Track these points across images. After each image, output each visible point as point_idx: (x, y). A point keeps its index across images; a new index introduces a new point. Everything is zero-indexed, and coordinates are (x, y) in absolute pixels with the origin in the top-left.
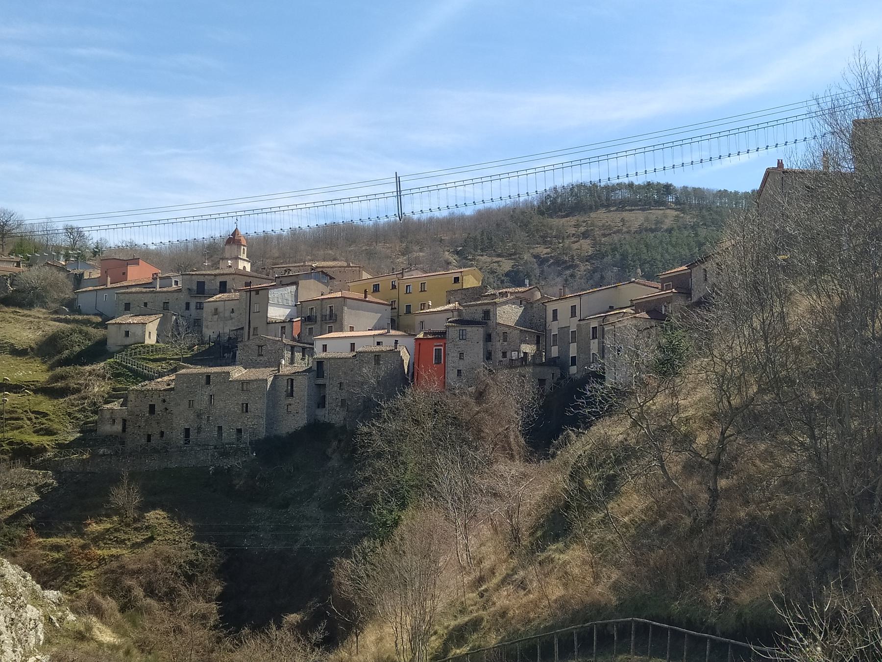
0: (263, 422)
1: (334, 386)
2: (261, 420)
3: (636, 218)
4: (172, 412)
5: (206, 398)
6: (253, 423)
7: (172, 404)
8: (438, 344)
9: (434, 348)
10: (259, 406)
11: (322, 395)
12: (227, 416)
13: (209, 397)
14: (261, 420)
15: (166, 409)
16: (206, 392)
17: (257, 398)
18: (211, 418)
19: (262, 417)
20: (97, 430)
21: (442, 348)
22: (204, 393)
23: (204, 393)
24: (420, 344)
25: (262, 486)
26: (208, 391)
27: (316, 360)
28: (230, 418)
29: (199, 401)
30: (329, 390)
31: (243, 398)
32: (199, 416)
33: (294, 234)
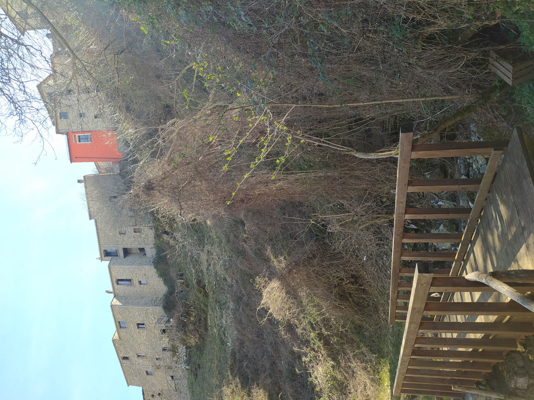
0: (151, 309)
1: (123, 240)
2: (149, 311)
4: (161, 390)
5: (141, 360)
6: (153, 318)
7: (154, 389)
8: (74, 139)
9: (78, 143)
10: (137, 313)
11: (139, 252)
12: (151, 342)
13: (139, 358)
14: (149, 311)
15: (159, 394)
16: (136, 361)
17: (130, 315)
18: (157, 357)
19: (146, 310)
20: (425, 243)
21: (77, 135)
22: (137, 362)
23: (137, 362)
24: (76, 157)
25: (194, 315)
26: (134, 359)
27: (103, 257)
28: (153, 340)
29: (145, 367)
30: (128, 245)
31: (133, 327)
32: (158, 367)
33: (160, 275)
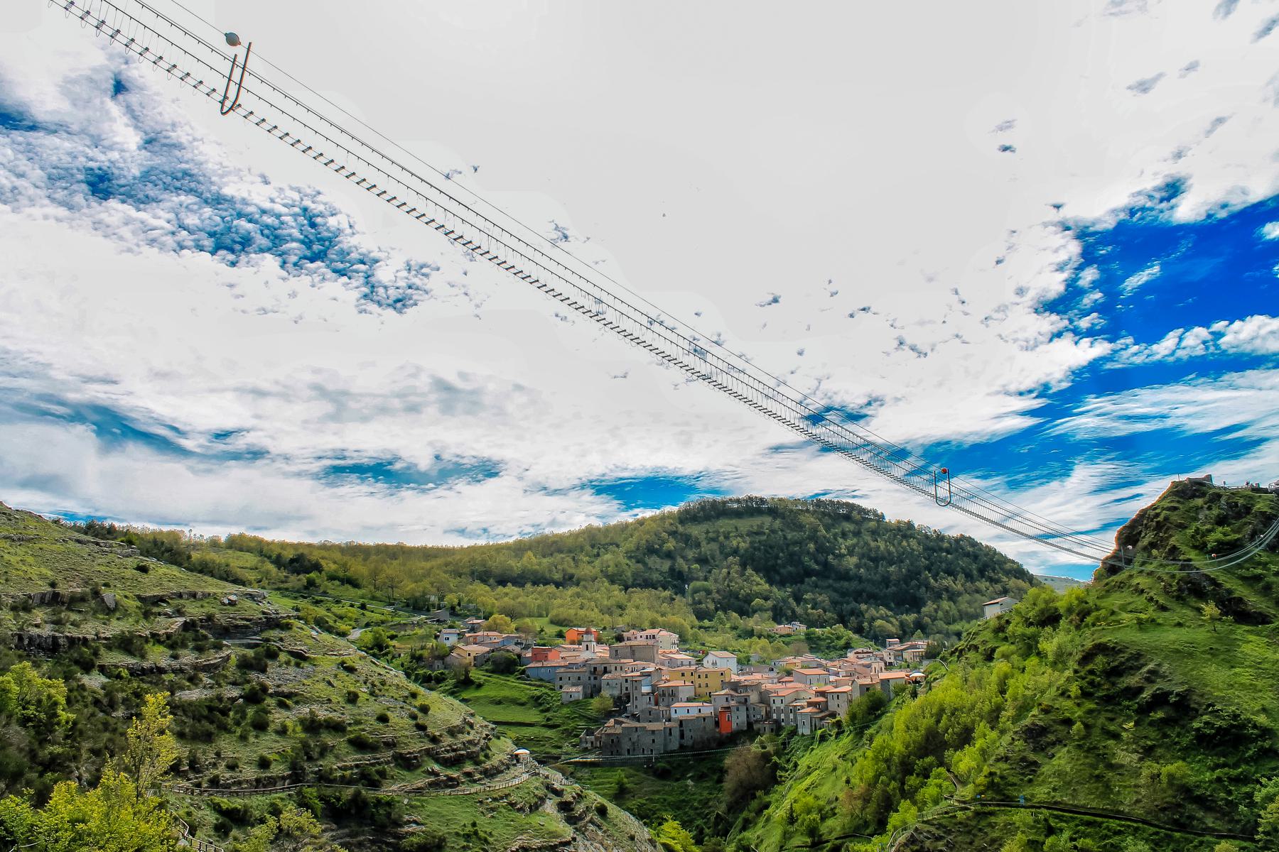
3: (745, 524)
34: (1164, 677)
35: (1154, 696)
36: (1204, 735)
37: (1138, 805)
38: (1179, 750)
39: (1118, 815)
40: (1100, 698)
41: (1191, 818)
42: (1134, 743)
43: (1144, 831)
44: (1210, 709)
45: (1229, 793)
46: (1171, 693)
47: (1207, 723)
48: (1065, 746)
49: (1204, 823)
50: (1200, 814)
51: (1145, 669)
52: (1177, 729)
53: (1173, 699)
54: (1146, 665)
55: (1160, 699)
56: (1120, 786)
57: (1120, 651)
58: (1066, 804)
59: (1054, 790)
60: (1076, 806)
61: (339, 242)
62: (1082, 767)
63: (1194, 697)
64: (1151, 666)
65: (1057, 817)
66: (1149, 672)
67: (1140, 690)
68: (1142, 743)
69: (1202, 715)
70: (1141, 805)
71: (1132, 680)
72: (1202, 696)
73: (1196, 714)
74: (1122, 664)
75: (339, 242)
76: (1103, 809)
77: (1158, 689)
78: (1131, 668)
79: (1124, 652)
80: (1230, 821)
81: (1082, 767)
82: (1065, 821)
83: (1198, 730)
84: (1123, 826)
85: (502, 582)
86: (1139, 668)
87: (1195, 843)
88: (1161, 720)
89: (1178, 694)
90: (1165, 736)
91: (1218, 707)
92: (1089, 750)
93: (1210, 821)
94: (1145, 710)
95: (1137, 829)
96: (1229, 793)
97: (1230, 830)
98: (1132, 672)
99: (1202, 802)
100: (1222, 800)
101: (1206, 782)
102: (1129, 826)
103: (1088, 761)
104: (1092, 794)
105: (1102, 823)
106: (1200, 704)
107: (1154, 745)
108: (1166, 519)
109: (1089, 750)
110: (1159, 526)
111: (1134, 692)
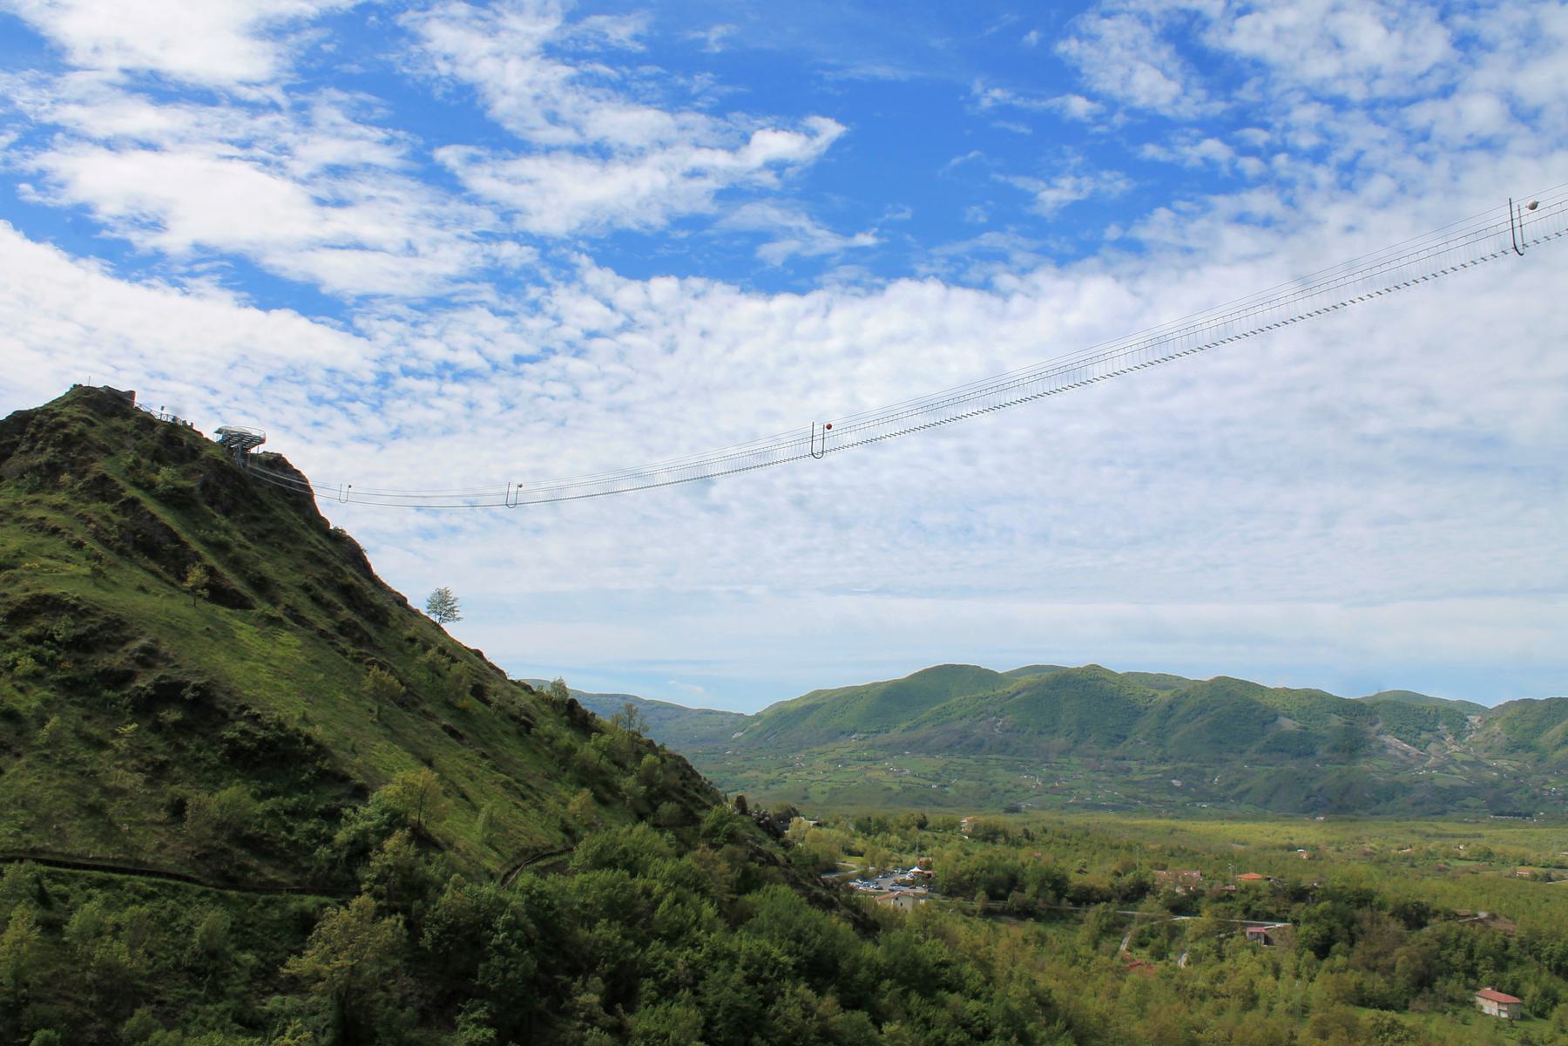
34: (168, 660)
35: (157, 686)
36: (243, 749)
37: (165, 851)
38: (206, 770)
39: (140, 869)
40: (61, 682)
41: (244, 868)
42: (132, 756)
43: (187, 891)
44: (245, 713)
45: (290, 830)
46: (186, 684)
47: (243, 732)
48: (18, 756)
49: (261, 875)
50: (254, 862)
51: (135, 645)
52: (198, 740)
53: (189, 695)
54: (134, 639)
55: (168, 693)
56: (130, 823)
57: (87, 612)
58: (52, 853)
59: (25, 828)
60: (69, 855)
61: (1094, 38)
62: (60, 792)
63: (220, 695)
64: (144, 641)
65: (49, 875)
66: (143, 649)
67: (128, 677)
68: (147, 757)
69: (233, 721)
70: (168, 851)
71: (116, 660)
72: (229, 693)
73: (225, 719)
74: (92, 632)
75: (1094, 38)
76: (114, 860)
77: (162, 677)
78: (108, 641)
79: (93, 615)
80: (295, 871)
81: (60, 792)
82: (63, 882)
83: (232, 741)
84: (154, 884)
85: (522, 182)
86: (123, 643)
87: (260, 903)
88: (176, 724)
89: (196, 688)
90: (180, 748)
91: (257, 711)
92: (64, 765)
93: (270, 873)
94: (145, 707)
95: (176, 888)
96: (290, 830)
97: (297, 883)
98: (111, 647)
99: (254, 844)
100: (282, 840)
101: (257, 816)
102: (163, 885)
103: (66, 781)
104: (90, 835)
105: (122, 882)
106: (229, 706)
107: (166, 761)
108: (82, 434)
109: (64, 765)
110: (68, 442)
111: (120, 679)
